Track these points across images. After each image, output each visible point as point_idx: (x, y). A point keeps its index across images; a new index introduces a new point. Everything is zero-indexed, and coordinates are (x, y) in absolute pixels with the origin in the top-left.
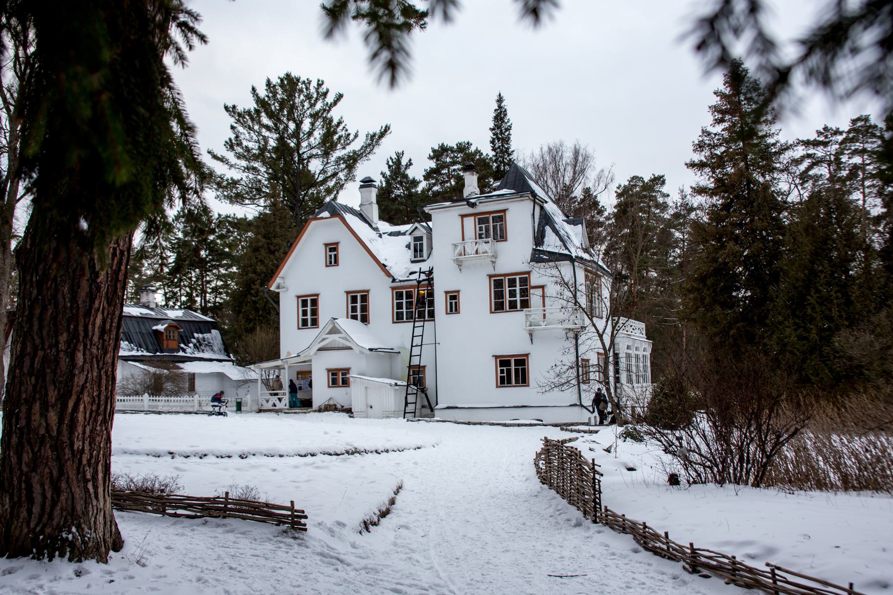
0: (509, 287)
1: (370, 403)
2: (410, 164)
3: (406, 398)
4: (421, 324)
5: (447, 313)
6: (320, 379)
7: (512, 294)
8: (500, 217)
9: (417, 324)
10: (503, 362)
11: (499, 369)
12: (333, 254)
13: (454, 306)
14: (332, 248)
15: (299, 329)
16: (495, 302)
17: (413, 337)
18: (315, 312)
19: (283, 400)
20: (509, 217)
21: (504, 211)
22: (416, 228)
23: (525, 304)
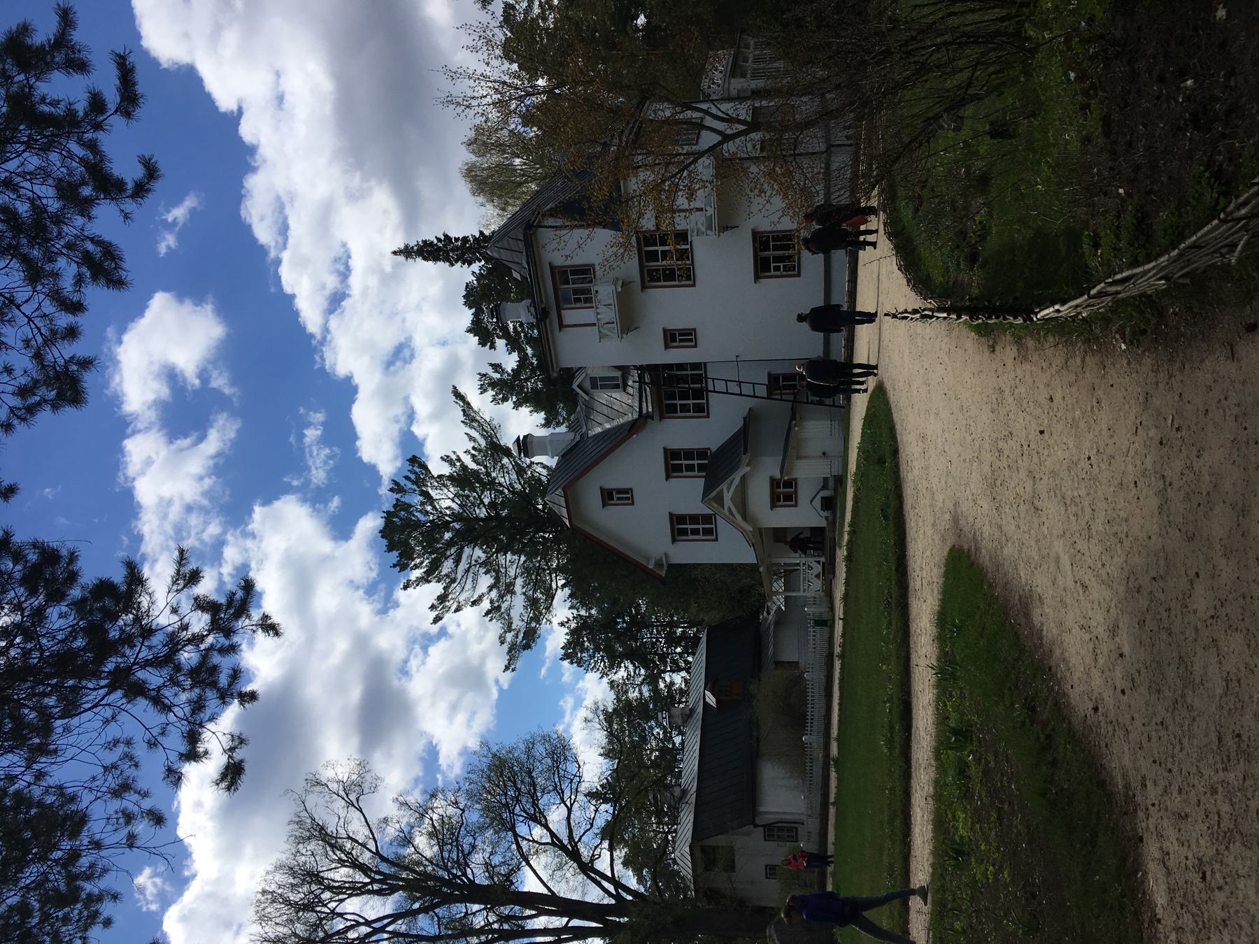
2: (497, 367)
4: (710, 382)
5: (695, 346)
6: (785, 518)
9: (711, 388)
10: (762, 268)
11: (773, 273)
12: (615, 496)
14: (608, 496)
15: (716, 540)
17: (727, 393)
18: (694, 519)
20: (559, 261)
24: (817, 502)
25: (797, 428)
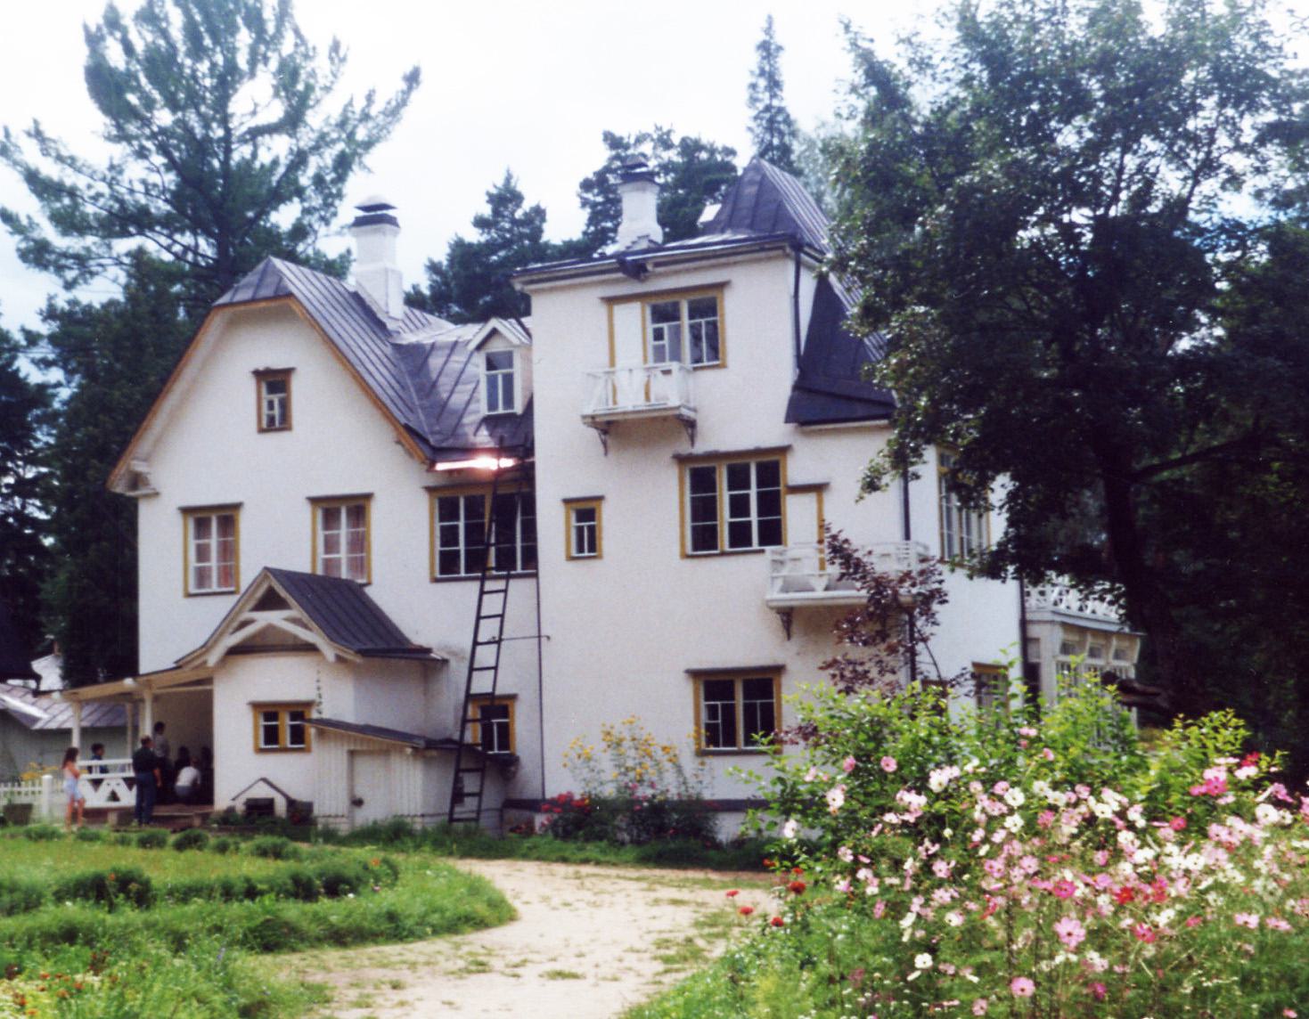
0: (730, 488)
1: (360, 792)
3: (457, 781)
4: (500, 585)
7: (739, 506)
8: (706, 306)
9: (489, 585)
13: (587, 541)
14: (275, 381)
16: (724, 745)
17: (479, 618)
19: (104, 783)
21: (721, 286)
22: (494, 332)
23: (773, 534)
24: (262, 792)
25: (409, 751)
